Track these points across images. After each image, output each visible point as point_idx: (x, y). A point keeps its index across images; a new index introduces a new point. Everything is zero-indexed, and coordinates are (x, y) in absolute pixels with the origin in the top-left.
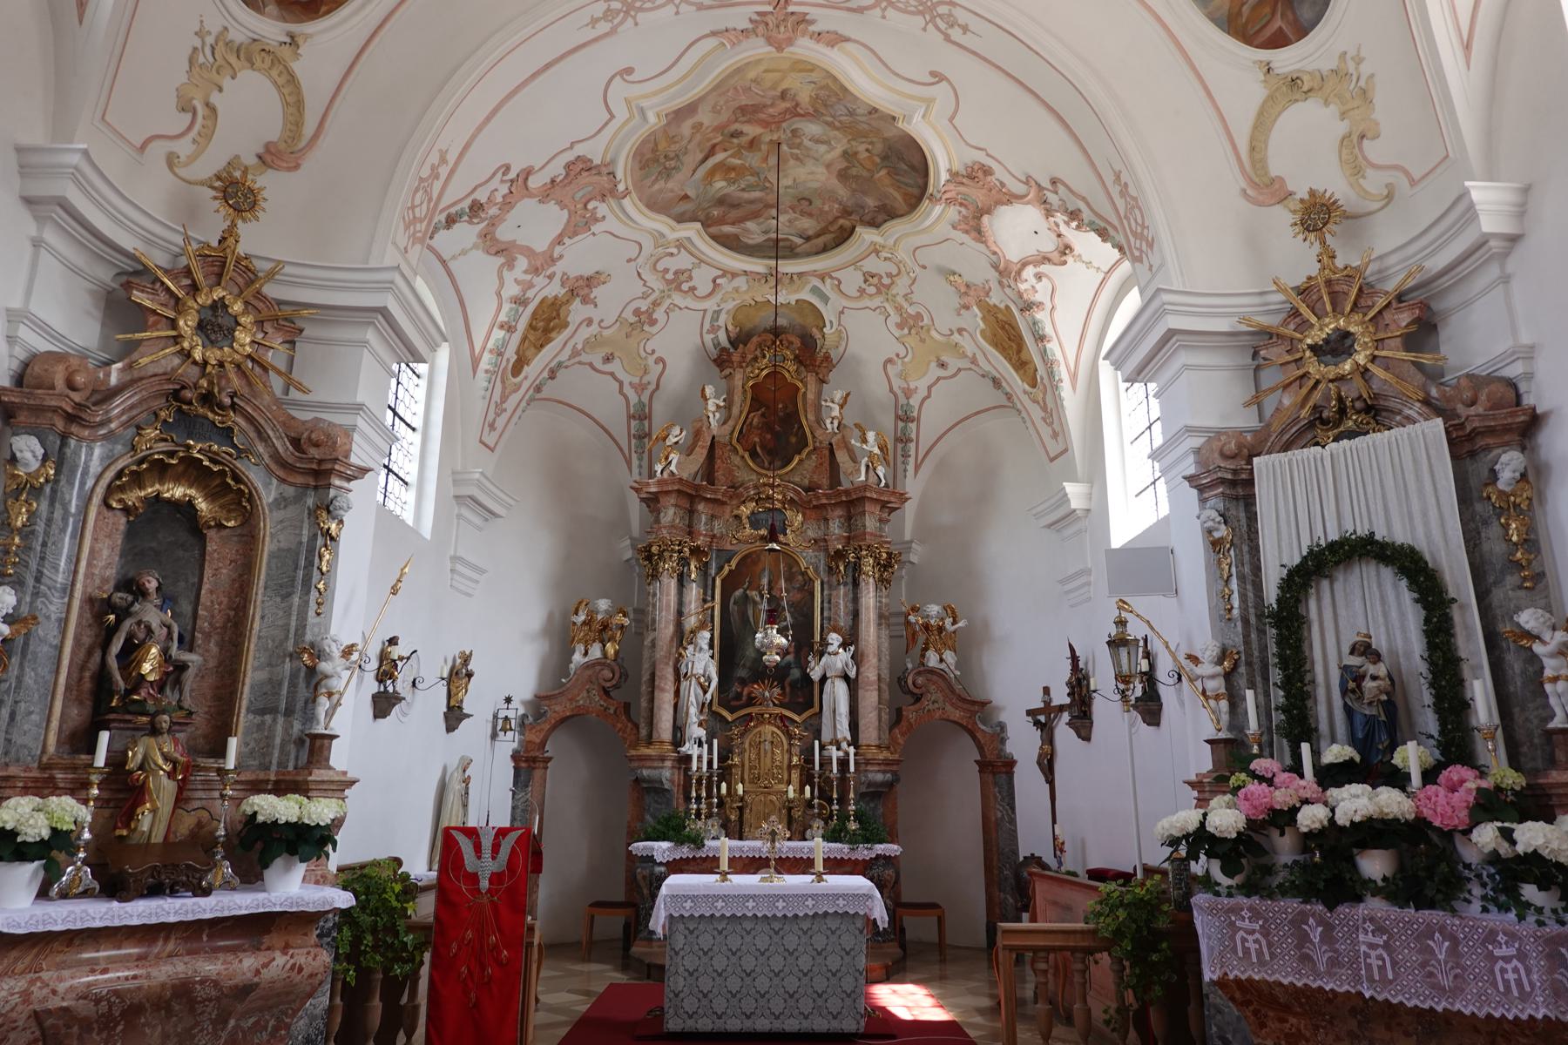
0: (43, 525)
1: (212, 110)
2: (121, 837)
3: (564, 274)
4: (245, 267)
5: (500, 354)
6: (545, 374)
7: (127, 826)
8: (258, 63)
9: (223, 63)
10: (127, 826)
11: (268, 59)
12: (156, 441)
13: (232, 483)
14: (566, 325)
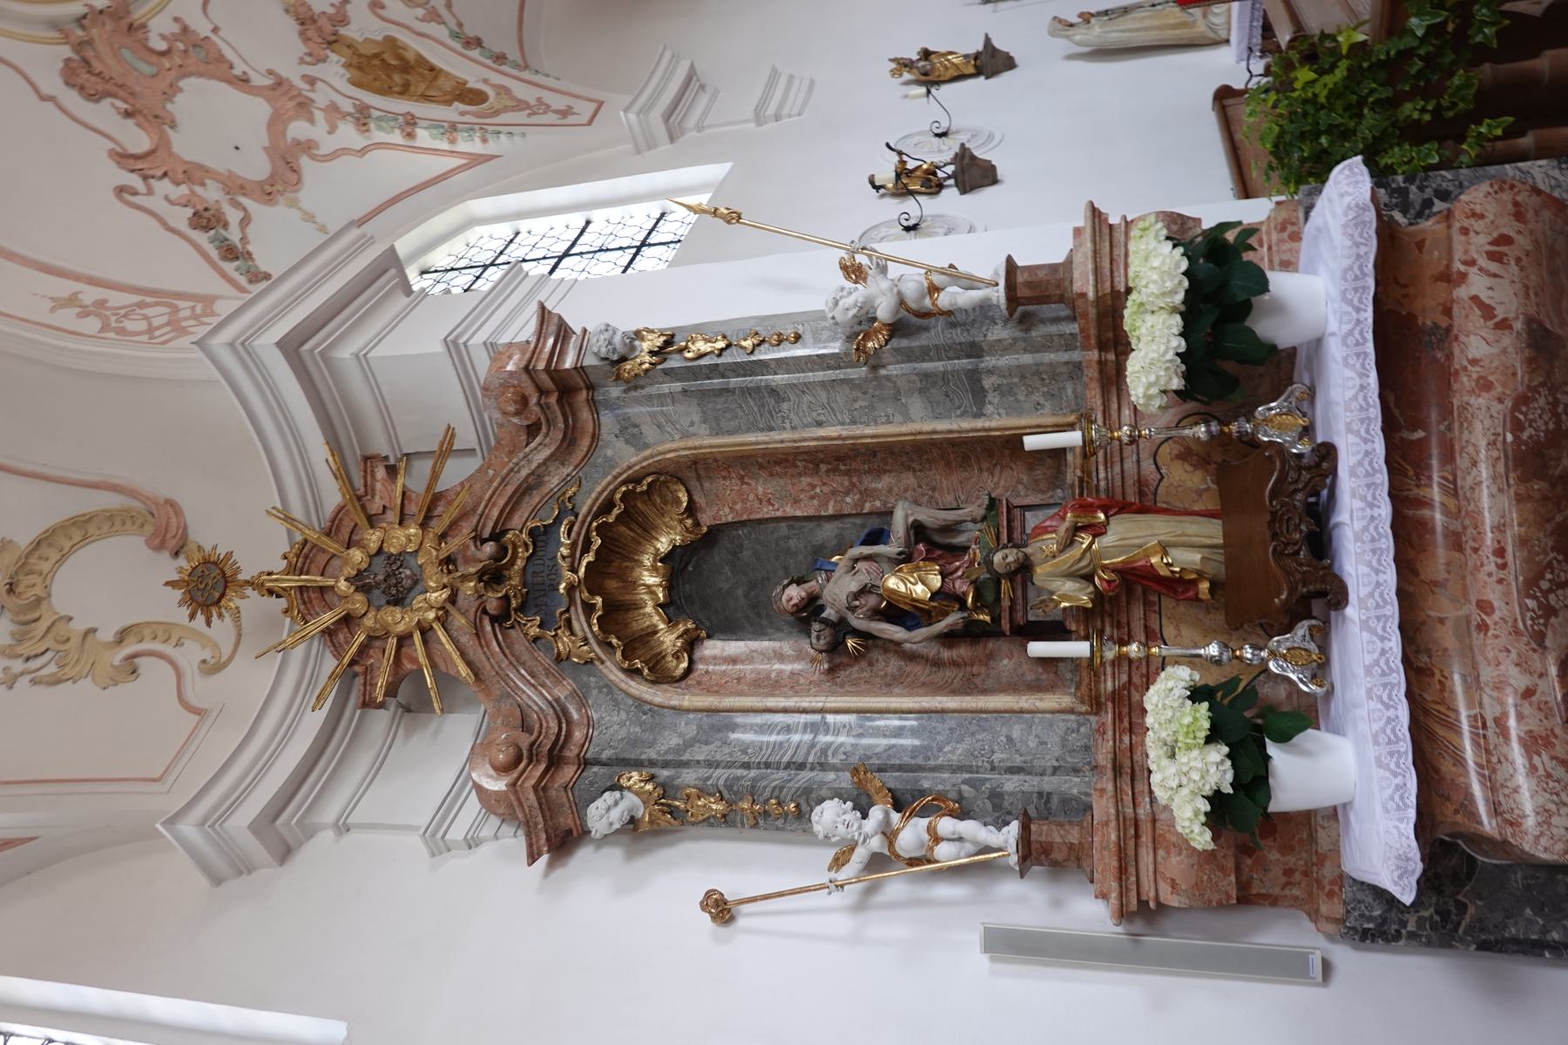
0: (719, 771)
1: (122, 636)
2: (1212, 590)
3: (302, 61)
4: (303, 557)
5: (453, 127)
6: (475, 53)
7: (1194, 583)
8: (38, 591)
9: (50, 636)
10: (1194, 583)
11: (25, 581)
12: (573, 633)
13: (616, 511)
14: (390, 41)
